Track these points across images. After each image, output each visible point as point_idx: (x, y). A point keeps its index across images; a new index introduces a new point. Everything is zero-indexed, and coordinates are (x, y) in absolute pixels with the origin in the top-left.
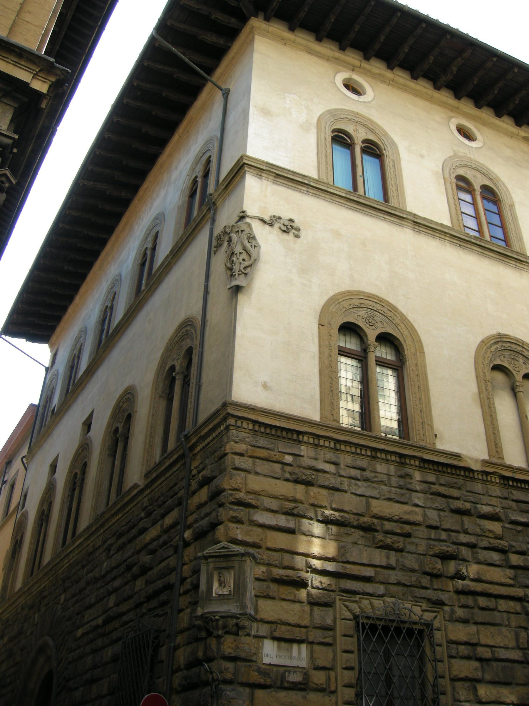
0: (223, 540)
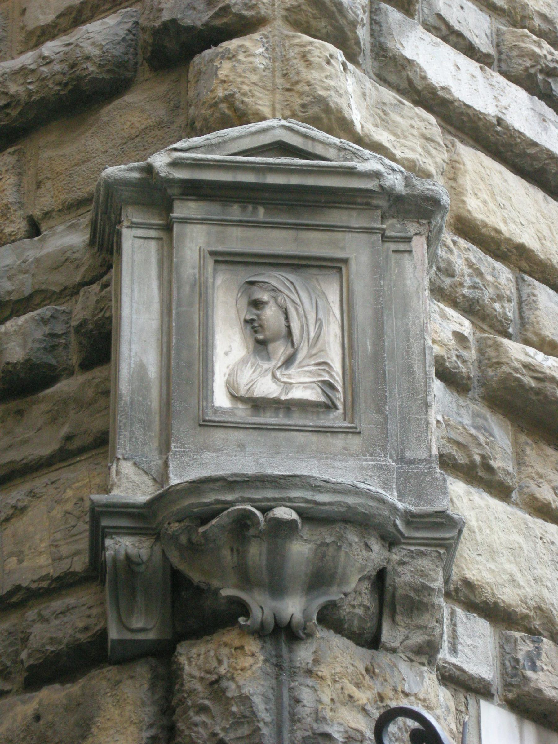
0: (266, 110)
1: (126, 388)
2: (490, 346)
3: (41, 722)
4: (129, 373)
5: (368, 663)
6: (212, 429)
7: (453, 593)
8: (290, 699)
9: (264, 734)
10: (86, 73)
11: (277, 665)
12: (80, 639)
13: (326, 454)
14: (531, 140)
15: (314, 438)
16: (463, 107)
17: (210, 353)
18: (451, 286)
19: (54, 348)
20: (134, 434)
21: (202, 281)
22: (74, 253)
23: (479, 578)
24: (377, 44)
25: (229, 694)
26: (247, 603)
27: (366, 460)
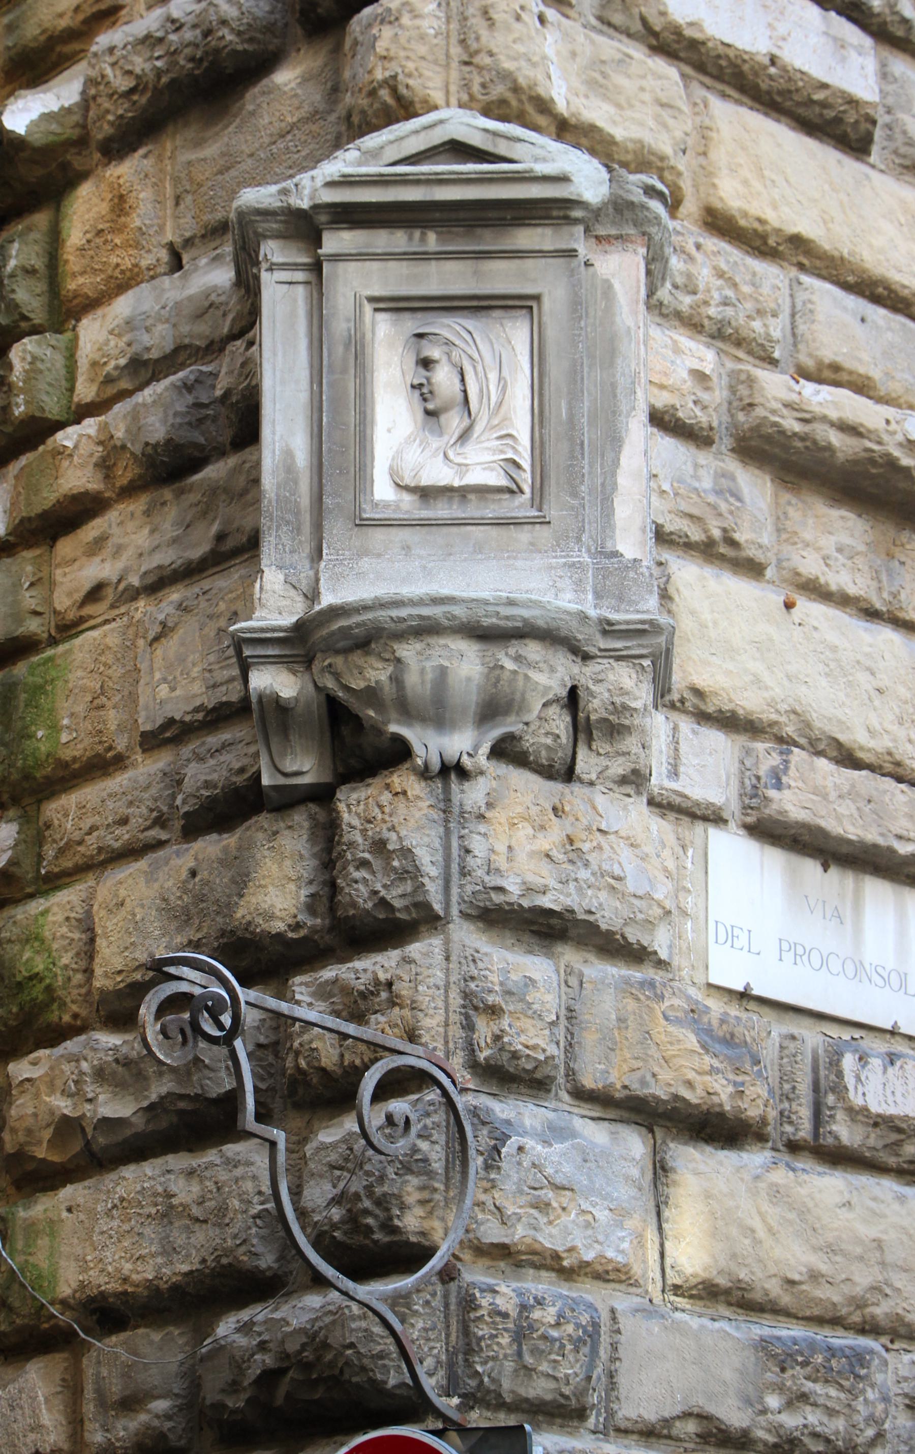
0: (437, 96)
2: (743, 382)
3: (197, 879)
6: (371, 530)
7: (678, 704)
10: (223, 43)
14: (819, 82)
15: (493, 532)
16: (720, 47)
18: (691, 307)
19: (200, 421)
20: (280, 539)
22: (219, 295)
25: (390, 847)
27: (556, 557)
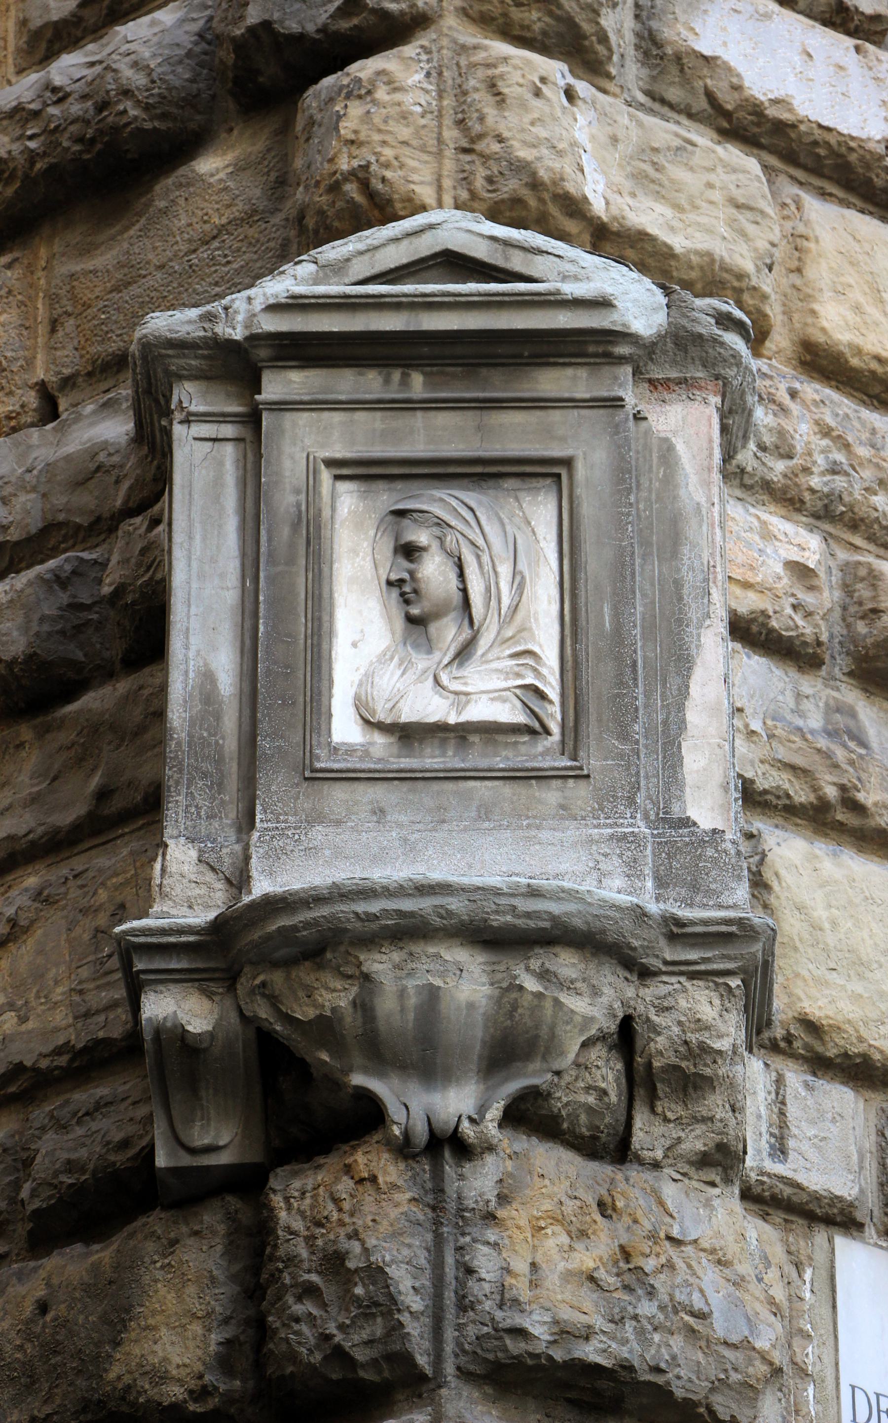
0: (426, 194)
1: (179, 717)
2: (862, 579)
4: (185, 689)
5: (604, 1192)
8: (457, 1269)
9: (408, 1334)
10: (125, 120)
11: (434, 1209)
12: (114, 1163)
13: (528, 818)
15: (507, 789)
16: (817, 131)
17: (325, 646)
18: (785, 476)
19: (78, 629)
20: (193, 798)
21: (311, 516)
22: (110, 455)
23: (831, 1014)
24: (646, 34)
25: (351, 1265)
26: (381, 1100)
27: (598, 826)
